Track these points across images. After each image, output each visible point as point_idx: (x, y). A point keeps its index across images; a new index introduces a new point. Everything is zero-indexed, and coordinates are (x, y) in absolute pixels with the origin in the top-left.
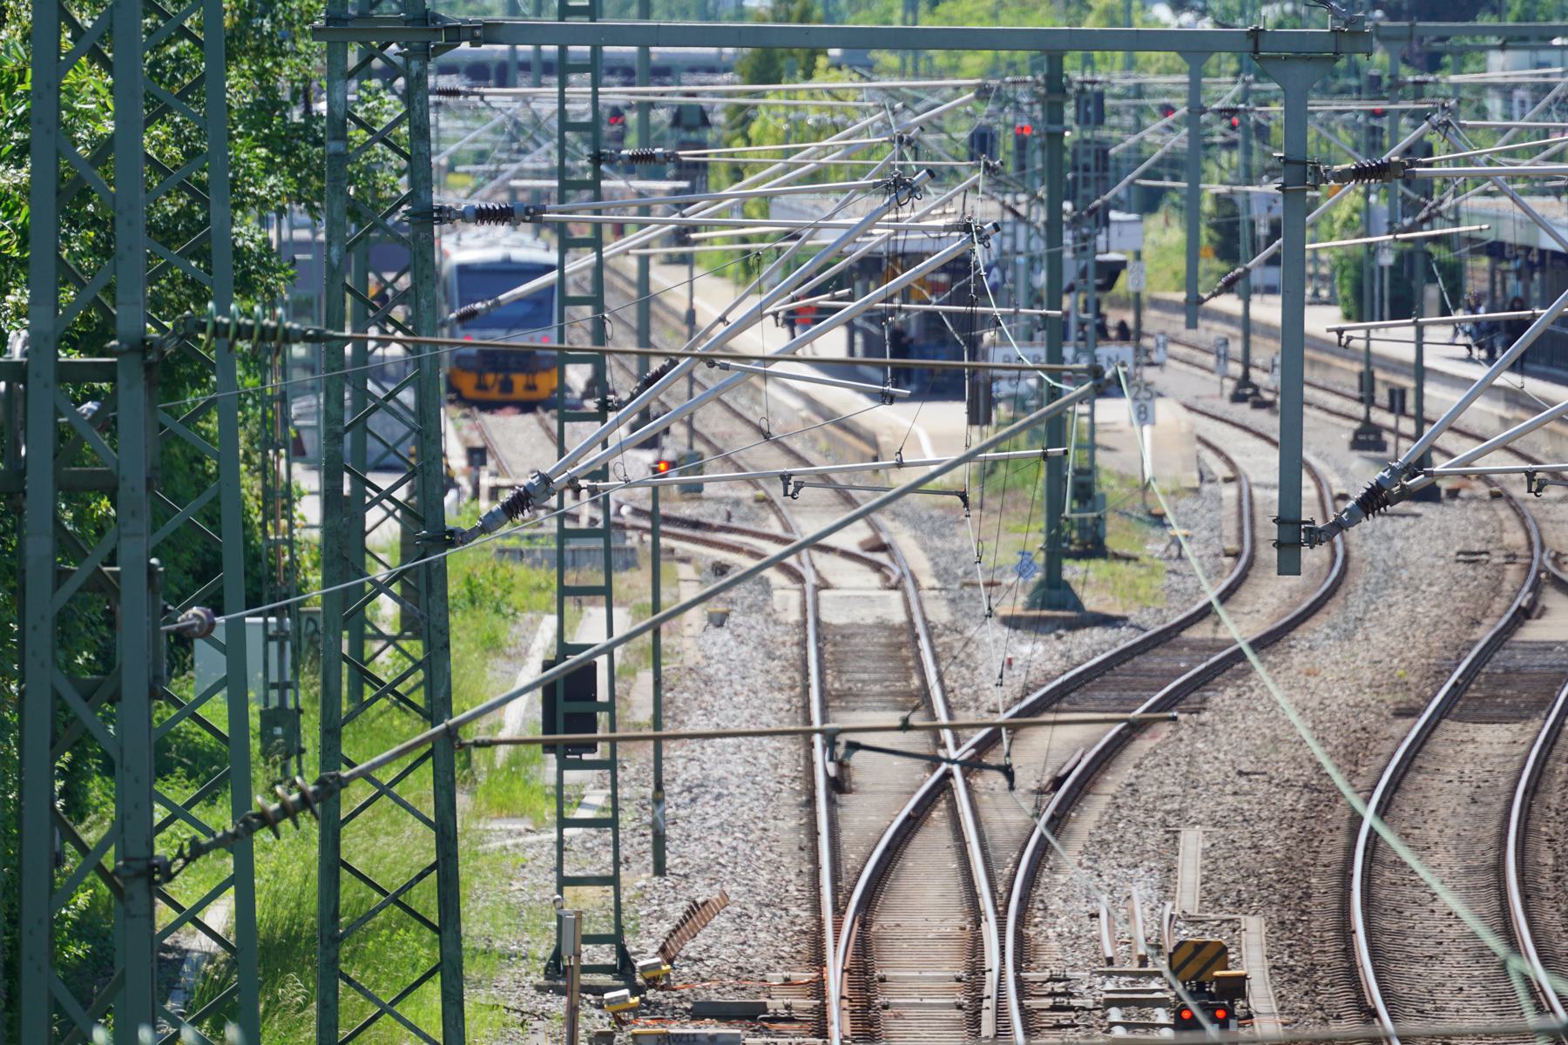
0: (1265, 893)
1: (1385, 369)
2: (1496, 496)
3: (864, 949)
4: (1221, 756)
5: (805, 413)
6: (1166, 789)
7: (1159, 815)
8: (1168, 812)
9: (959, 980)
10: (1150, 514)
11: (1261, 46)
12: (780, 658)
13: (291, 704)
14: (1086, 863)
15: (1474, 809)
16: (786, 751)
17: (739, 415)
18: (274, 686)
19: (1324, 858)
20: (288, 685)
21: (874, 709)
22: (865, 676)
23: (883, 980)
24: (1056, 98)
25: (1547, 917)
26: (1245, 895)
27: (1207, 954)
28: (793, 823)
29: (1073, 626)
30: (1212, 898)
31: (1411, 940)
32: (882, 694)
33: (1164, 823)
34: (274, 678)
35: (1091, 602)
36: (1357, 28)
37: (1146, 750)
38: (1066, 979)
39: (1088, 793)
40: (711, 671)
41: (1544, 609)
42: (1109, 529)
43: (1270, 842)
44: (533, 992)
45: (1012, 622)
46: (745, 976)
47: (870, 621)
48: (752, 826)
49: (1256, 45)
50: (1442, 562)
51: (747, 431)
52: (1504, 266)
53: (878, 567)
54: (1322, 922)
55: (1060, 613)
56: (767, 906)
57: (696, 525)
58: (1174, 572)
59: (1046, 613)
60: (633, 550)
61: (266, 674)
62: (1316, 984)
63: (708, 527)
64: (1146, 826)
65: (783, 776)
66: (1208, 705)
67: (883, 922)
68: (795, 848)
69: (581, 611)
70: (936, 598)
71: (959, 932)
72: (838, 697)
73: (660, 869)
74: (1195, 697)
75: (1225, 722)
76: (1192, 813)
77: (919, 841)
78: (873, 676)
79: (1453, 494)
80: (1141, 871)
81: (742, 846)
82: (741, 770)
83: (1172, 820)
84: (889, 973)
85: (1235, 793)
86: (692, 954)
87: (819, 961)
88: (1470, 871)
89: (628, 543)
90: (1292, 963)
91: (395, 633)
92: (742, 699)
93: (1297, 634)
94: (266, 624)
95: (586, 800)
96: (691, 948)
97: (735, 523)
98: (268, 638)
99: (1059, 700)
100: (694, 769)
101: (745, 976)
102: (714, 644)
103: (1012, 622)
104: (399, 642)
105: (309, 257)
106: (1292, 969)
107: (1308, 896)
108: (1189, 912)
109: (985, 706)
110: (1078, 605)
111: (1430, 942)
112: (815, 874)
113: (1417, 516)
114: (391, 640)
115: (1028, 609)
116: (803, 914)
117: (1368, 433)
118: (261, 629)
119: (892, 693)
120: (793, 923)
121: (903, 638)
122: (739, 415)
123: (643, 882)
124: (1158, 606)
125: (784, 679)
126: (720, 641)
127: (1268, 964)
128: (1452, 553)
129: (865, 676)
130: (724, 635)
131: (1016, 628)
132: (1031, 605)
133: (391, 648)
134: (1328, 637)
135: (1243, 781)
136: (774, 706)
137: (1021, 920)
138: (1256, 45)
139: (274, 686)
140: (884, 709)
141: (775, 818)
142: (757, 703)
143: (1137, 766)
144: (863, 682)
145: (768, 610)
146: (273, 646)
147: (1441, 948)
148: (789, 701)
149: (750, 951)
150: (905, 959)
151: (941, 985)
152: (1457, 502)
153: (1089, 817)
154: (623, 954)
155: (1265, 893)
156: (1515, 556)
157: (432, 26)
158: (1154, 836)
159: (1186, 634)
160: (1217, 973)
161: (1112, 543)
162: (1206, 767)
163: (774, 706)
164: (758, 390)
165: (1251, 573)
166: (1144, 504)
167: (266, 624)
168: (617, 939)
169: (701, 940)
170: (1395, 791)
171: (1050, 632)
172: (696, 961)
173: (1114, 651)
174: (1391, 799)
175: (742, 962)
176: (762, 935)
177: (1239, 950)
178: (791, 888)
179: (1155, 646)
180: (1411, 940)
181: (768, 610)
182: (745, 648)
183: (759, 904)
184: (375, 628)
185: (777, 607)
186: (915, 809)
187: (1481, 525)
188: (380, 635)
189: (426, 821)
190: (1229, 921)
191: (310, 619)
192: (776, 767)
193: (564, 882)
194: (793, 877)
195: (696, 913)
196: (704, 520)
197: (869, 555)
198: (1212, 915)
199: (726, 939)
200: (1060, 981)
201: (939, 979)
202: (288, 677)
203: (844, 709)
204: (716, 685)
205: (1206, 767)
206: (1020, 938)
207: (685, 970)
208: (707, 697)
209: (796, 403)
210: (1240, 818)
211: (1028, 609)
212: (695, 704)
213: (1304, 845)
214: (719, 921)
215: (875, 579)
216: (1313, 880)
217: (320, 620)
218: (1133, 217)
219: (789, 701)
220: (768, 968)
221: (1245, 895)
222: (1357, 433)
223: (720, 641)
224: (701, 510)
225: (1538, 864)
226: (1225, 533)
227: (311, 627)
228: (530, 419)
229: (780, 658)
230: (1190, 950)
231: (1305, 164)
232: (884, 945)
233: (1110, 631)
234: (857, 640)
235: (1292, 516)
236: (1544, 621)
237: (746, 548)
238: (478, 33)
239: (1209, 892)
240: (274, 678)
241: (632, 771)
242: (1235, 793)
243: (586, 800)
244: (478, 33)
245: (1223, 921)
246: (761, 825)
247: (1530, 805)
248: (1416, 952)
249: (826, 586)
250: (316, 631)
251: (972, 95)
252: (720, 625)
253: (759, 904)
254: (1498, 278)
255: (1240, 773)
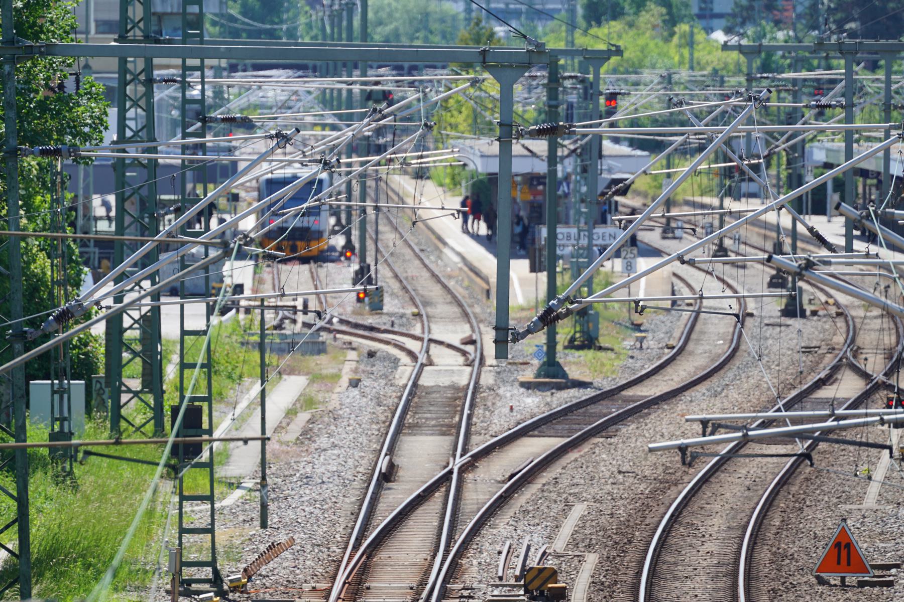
0: (605, 540)
1: (803, 241)
2: (839, 314)
3: (364, 569)
4: (614, 462)
5: (461, 265)
6: (575, 481)
7: (565, 496)
8: (570, 494)
9: (411, 588)
10: (633, 324)
11: (487, 60)
12: (385, 405)
13: (66, 430)
14: (512, 522)
15: (747, 493)
16: (366, 459)
17: (426, 266)
18: (57, 419)
19: (647, 521)
20: (65, 419)
21: (427, 435)
22: (429, 416)
23: (368, 588)
24: (553, 85)
25: (762, 555)
26: (594, 542)
27: (545, 574)
28: (354, 499)
29: (560, 387)
30: (574, 543)
31: (680, 568)
32: (433, 426)
33: (566, 500)
34: (57, 415)
35: (574, 373)
36: (541, 49)
37: (573, 459)
38: (472, 589)
39: (529, 483)
40: (341, 412)
41: (836, 379)
42: (601, 332)
43: (621, 512)
44: (164, 594)
45: (527, 386)
46: (291, 585)
47: (447, 384)
48: (328, 501)
49: (484, 58)
50: (790, 352)
51: (426, 274)
52: (869, 181)
53: (464, 353)
54: (631, 556)
55: (554, 380)
56: (319, 545)
57: (372, 329)
58: (632, 357)
59: (547, 380)
60: (323, 343)
61: (52, 412)
62: (614, 591)
63: (378, 330)
64: (556, 502)
65: (358, 472)
66: (618, 433)
67: (382, 555)
68: (349, 513)
69: (280, 378)
70: (490, 371)
71: (423, 561)
72: (409, 427)
73: (264, 525)
74: (613, 428)
75: (624, 442)
76: (585, 495)
77: (421, 510)
78: (434, 416)
79: (814, 313)
80: (539, 528)
81: (317, 511)
82: (335, 469)
83: (571, 498)
84: (373, 585)
85: (613, 484)
86: (264, 573)
87: (334, 578)
88: (730, 528)
89: (321, 339)
90: (604, 580)
91: (139, 389)
92: (351, 428)
93: (686, 393)
94: (52, 384)
95: (243, 485)
96: (263, 570)
97: (396, 329)
98: (54, 392)
99: (534, 430)
100: (309, 469)
101: (291, 585)
102: (348, 397)
103: (527, 386)
104: (140, 395)
105: (134, 174)
106: (602, 584)
107: (630, 542)
108: (558, 551)
109: (491, 433)
110: (564, 375)
111: (691, 569)
112: (441, 527)
113: (788, 326)
114: (136, 394)
115: (536, 378)
116: (338, 551)
117: (778, 279)
118: (50, 386)
119: (442, 426)
120: (329, 555)
121: (460, 394)
122: (426, 266)
123: (254, 532)
124: (614, 376)
125: (382, 418)
126: (351, 395)
127: (590, 580)
128: (798, 347)
129: (429, 416)
130: (355, 392)
131: (528, 388)
132: (538, 375)
133: (136, 399)
134: (704, 394)
135: (620, 477)
136: (369, 433)
137: (460, 554)
138: (484, 58)
139: (57, 419)
140: (432, 434)
141: (344, 496)
142: (359, 430)
143: (564, 468)
144: (427, 419)
145: (391, 377)
146: (56, 397)
147: (695, 572)
148: (379, 430)
149: (298, 571)
150: (386, 577)
151: (397, 591)
152: (815, 318)
153: (522, 499)
154: (216, 572)
155: (605, 540)
156: (834, 349)
157: (16, 45)
158: (557, 508)
159: (624, 393)
160: (550, 586)
161: (603, 341)
162: (603, 469)
163: (369, 433)
164: (441, 252)
165: (678, 358)
166: (630, 319)
167: (52, 384)
168: (213, 563)
169: (271, 565)
170: (704, 483)
171: (548, 390)
172: (264, 577)
173: (569, 404)
174: (701, 487)
175: (291, 578)
176: (308, 563)
177: (578, 572)
178: (338, 536)
179: (603, 399)
180: (680, 568)
181: (391, 377)
182: (365, 399)
183: (313, 545)
184: (126, 386)
185: (397, 376)
186: (424, 491)
187: (825, 330)
188: (129, 391)
189: (11, 496)
190: (578, 556)
191: (97, 381)
192: (356, 467)
193: (182, 531)
194: (341, 529)
195: (274, 549)
196: (374, 325)
197: (463, 347)
198: (570, 553)
199: (285, 564)
200: (468, 589)
201: (401, 588)
202: (66, 414)
203: (410, 434)
204: (340, 420)
205: (603, 469)
206: (454, 565)
207: (258, 582)
208: (333, 427)
209: (456, 259)
210: (610, 498)
211: (536, 378)
212: (324, 431)
213: (640, 514)
214: (287, 554)
215: (461, 359)
216: (637, 533)
217: (103, 381)
218: (646, 153)
219: (379, 430)
220: (305, 581)
221: (594, 542)
222: (772, 277)
223: (351, 395)
224: (379, 321)
225: (770, 524)
226: (674, 335)
227: (98, 386)
228: (306, 267)
229: (385, 405)
230: (536, 572)
231: (511, 126)
232: (378, 569)
233: (581, 390)
234: (434, 395)
235: (503, 325)
236: (835, 386)
237: (393, 342)
238: (42, 49)
239: (574, 540)
240: (57, 415)
241: (274, 469)
242: (613, 484)
243: (243, 485)
244: (42, 49)
245: (575, 556)
246: (334, 500)
247: (779, 491)
248: (680, 574)
249: (431, 363)
250: (101, 388)
251: (468, 84)
252: (356, 386)
253: (313, 545)
254: (867, 188)
255: (620, 472)
